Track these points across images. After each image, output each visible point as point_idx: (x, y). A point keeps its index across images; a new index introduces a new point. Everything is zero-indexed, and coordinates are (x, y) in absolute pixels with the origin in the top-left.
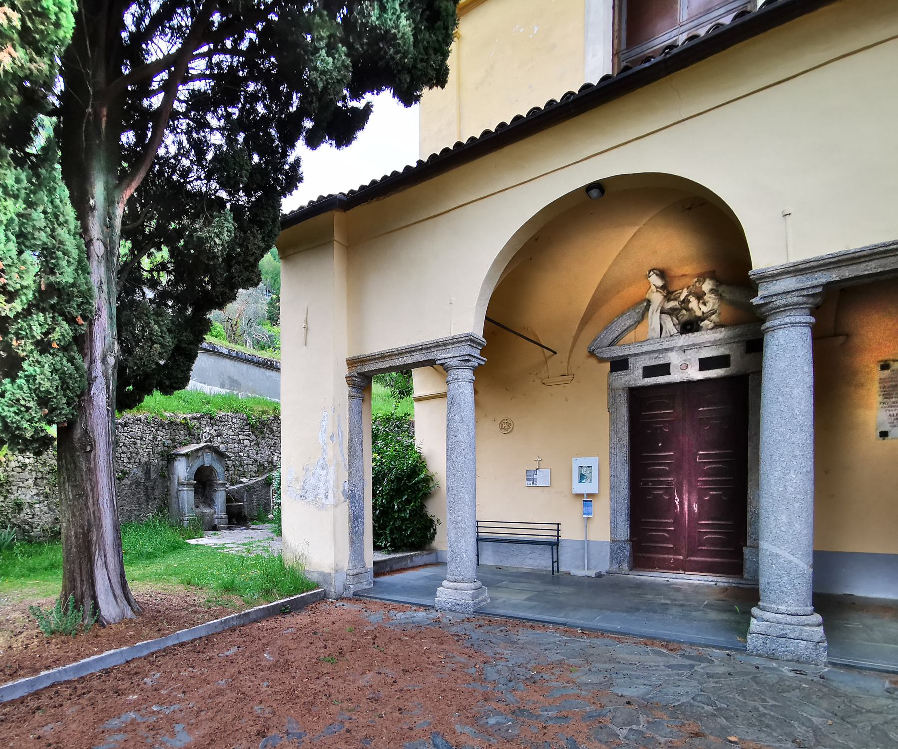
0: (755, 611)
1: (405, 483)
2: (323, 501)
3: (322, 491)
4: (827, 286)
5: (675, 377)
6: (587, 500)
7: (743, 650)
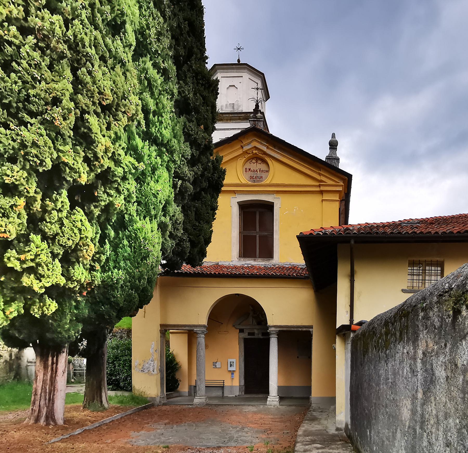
0: (269, 397)
1: (169, 366)
2: (152, 372)
3: (151, 369)
5: (256, 336)
6: (232, 372)
7: (266, 405)
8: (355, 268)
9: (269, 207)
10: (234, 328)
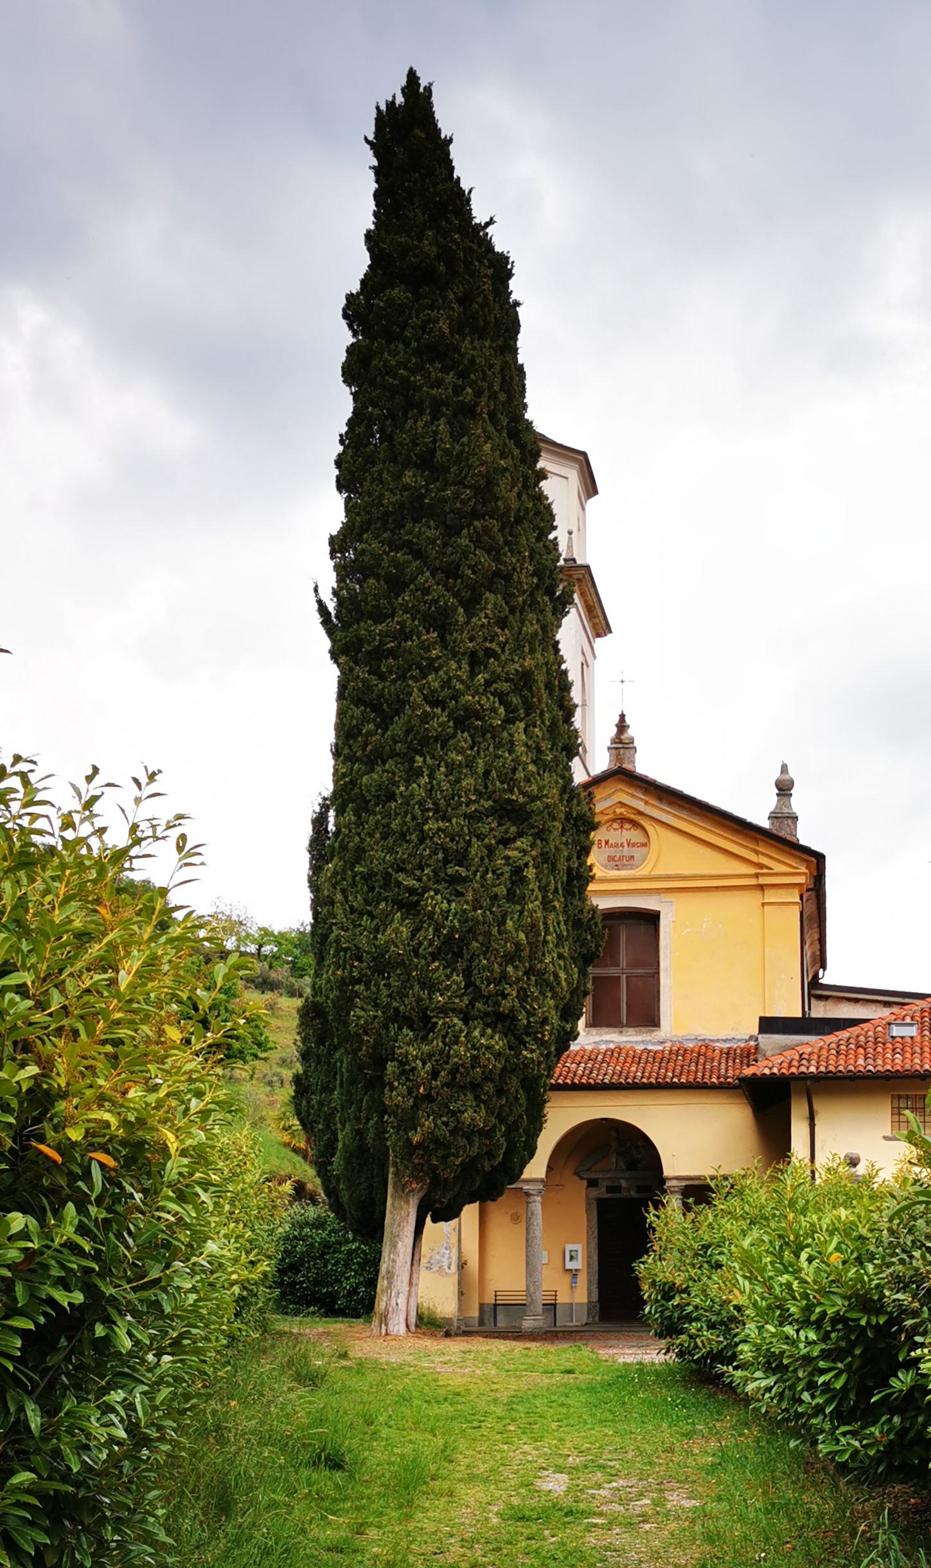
3: (445, 1264)
4: (686, 1186)
5: (624, 1195)
6: (574, 1274)
8: (815, 1107)
9: (652, 918)
10: (576, 1178)
